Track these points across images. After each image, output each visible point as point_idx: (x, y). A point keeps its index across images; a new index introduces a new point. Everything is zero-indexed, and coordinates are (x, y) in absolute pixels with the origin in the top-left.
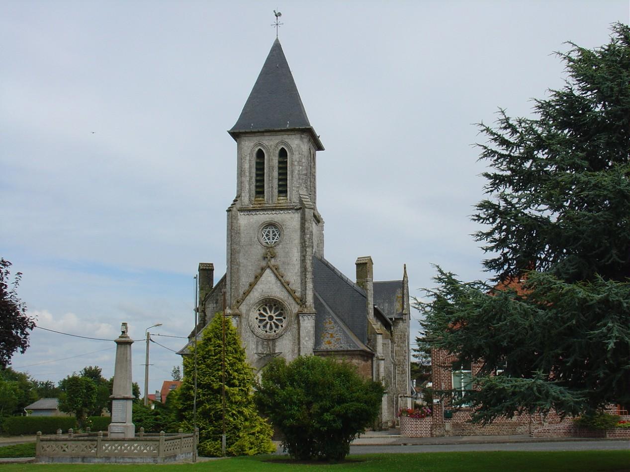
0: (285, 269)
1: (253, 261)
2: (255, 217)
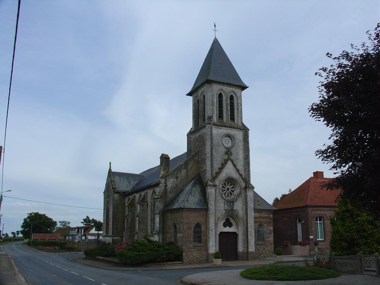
0: (236, 162)
1: (220, 155)
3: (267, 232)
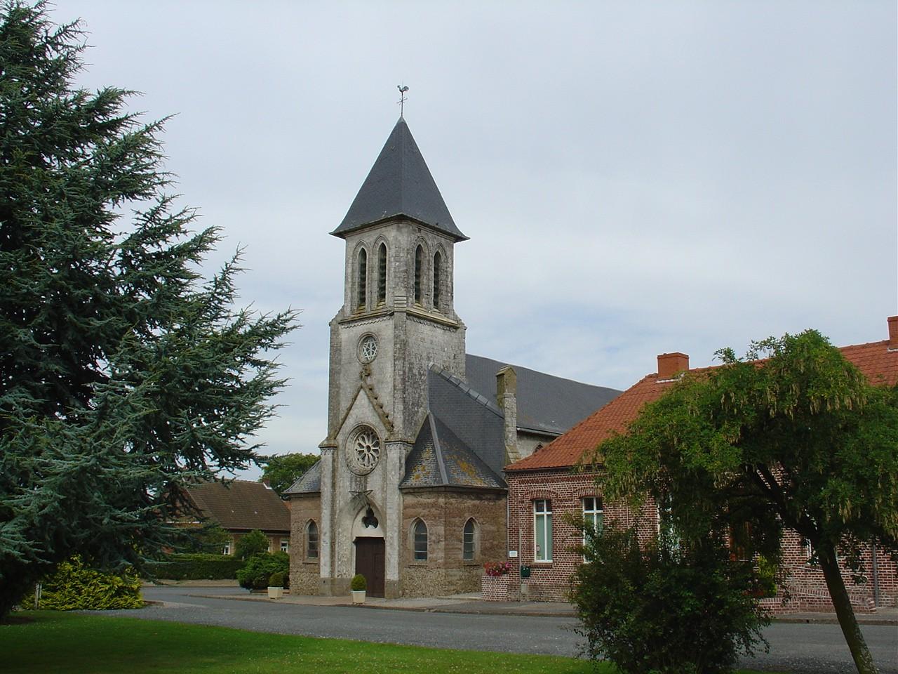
2: (355, 329)
3: (430, 539)
